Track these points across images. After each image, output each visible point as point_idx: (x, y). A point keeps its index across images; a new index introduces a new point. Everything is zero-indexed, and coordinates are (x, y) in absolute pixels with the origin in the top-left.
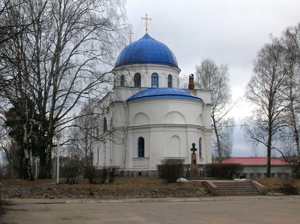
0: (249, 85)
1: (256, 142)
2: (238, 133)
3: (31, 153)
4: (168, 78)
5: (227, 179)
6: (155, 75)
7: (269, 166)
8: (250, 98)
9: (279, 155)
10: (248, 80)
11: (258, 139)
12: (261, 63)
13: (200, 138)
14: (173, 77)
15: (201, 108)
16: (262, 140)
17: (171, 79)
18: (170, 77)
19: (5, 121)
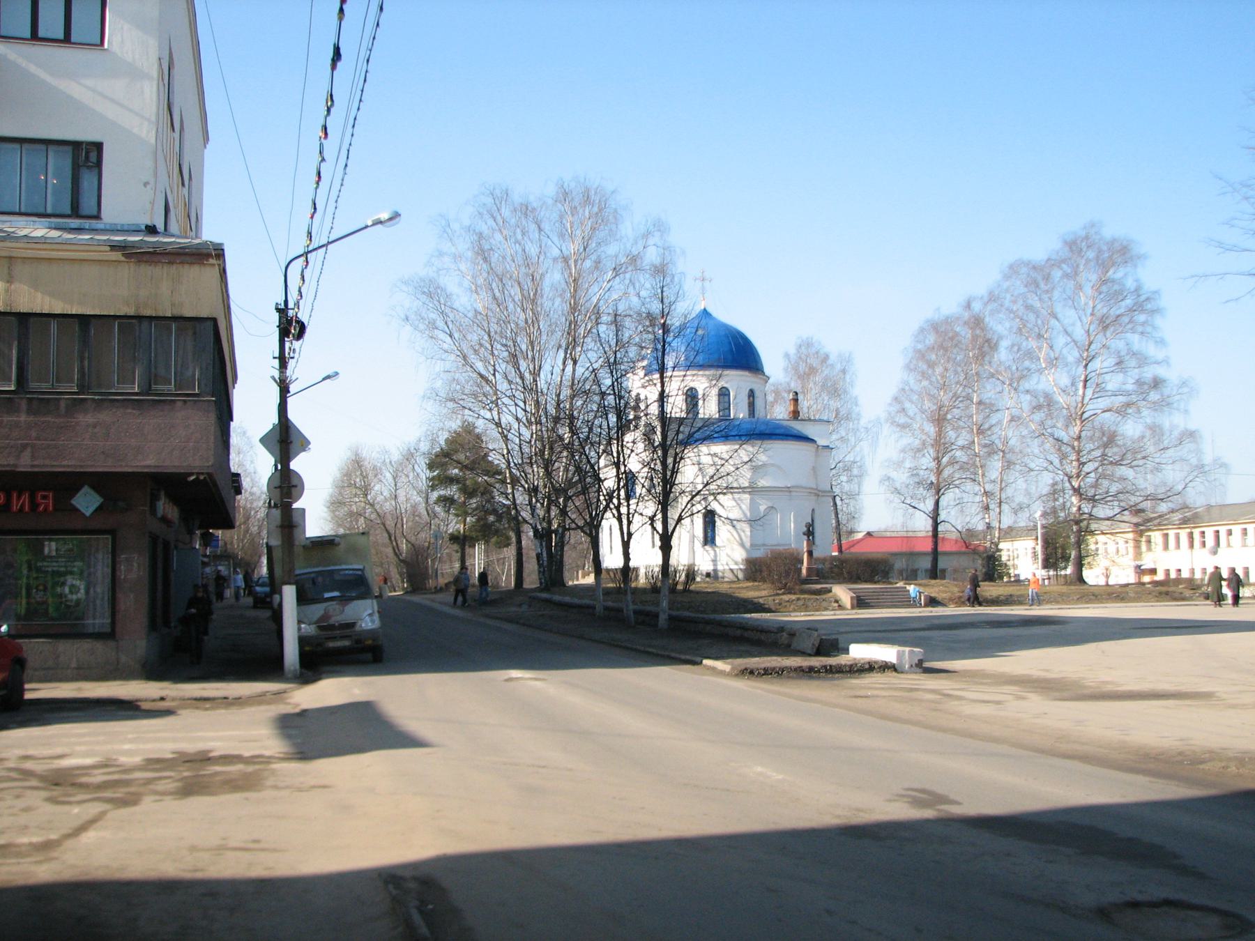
0: (896, 399)
1: (911, 510)
2: (431, 475)
3: (544, 544)
4: (749, 397)
5: (866, 581)
6: (724, 390)
7: (935, 553)
8: (898, 425)
9: (954, 536)
10: (893, 390)
11: (913, 504)
12: (921, 355)
13: (813, 510)
14: (757, 394)
15: (364, 454)
16: (921, 506)
17: (753, 397)
18: (752, 394)
19: (1132, 531)
